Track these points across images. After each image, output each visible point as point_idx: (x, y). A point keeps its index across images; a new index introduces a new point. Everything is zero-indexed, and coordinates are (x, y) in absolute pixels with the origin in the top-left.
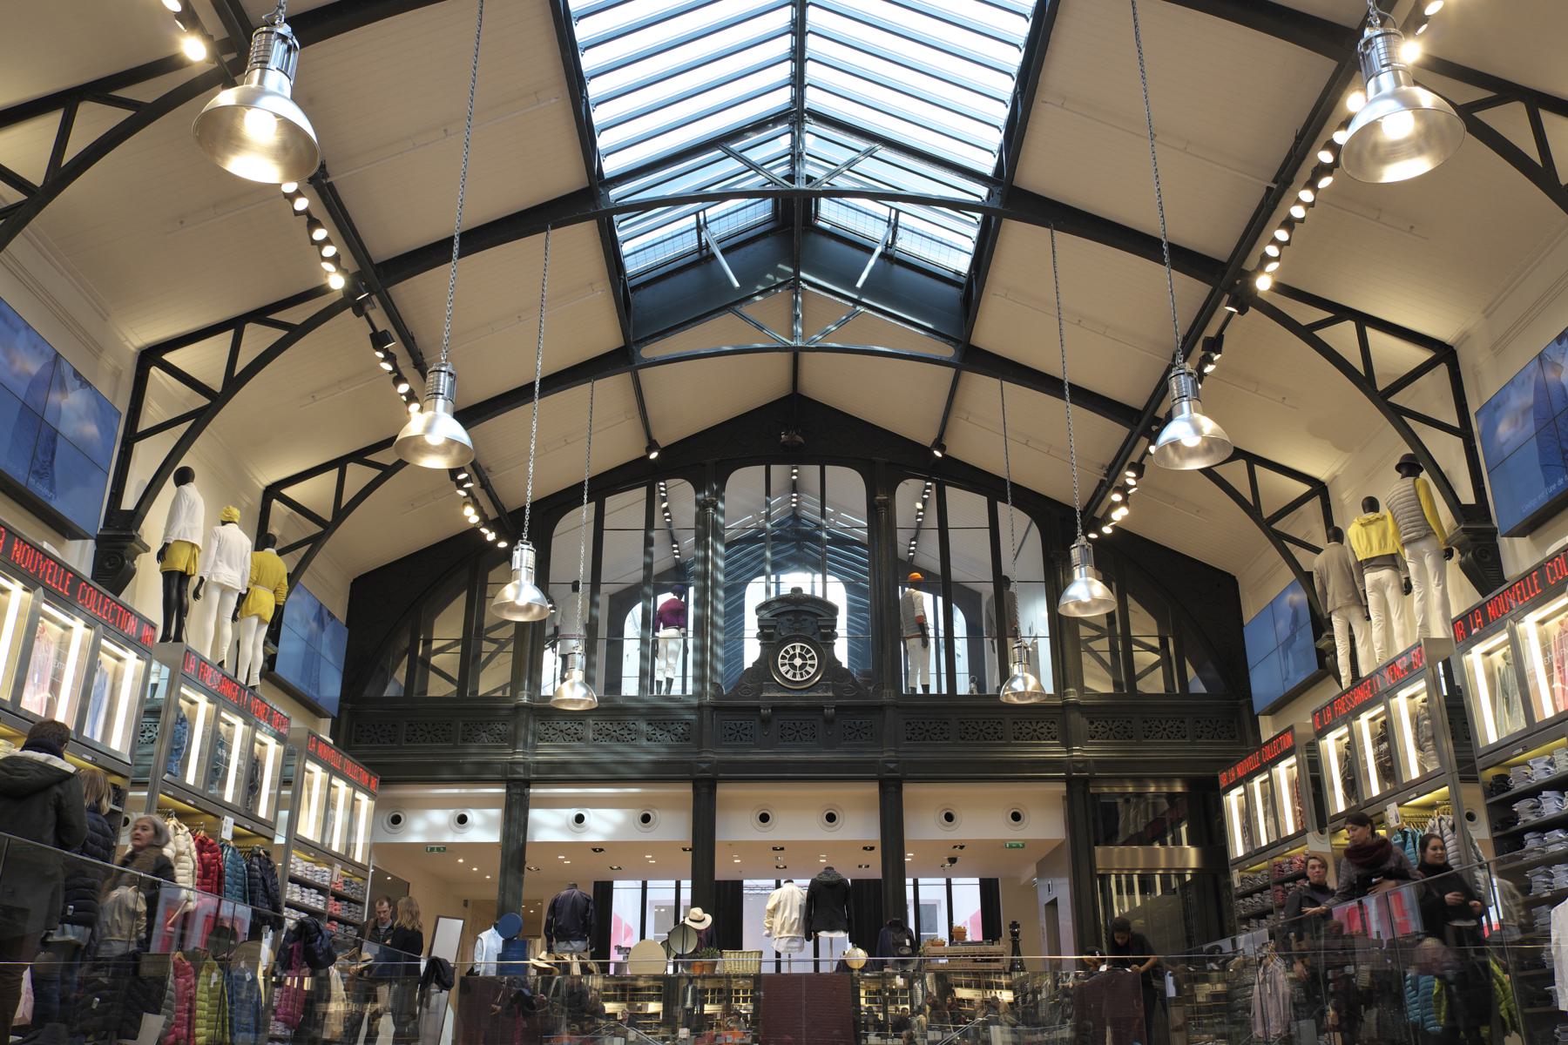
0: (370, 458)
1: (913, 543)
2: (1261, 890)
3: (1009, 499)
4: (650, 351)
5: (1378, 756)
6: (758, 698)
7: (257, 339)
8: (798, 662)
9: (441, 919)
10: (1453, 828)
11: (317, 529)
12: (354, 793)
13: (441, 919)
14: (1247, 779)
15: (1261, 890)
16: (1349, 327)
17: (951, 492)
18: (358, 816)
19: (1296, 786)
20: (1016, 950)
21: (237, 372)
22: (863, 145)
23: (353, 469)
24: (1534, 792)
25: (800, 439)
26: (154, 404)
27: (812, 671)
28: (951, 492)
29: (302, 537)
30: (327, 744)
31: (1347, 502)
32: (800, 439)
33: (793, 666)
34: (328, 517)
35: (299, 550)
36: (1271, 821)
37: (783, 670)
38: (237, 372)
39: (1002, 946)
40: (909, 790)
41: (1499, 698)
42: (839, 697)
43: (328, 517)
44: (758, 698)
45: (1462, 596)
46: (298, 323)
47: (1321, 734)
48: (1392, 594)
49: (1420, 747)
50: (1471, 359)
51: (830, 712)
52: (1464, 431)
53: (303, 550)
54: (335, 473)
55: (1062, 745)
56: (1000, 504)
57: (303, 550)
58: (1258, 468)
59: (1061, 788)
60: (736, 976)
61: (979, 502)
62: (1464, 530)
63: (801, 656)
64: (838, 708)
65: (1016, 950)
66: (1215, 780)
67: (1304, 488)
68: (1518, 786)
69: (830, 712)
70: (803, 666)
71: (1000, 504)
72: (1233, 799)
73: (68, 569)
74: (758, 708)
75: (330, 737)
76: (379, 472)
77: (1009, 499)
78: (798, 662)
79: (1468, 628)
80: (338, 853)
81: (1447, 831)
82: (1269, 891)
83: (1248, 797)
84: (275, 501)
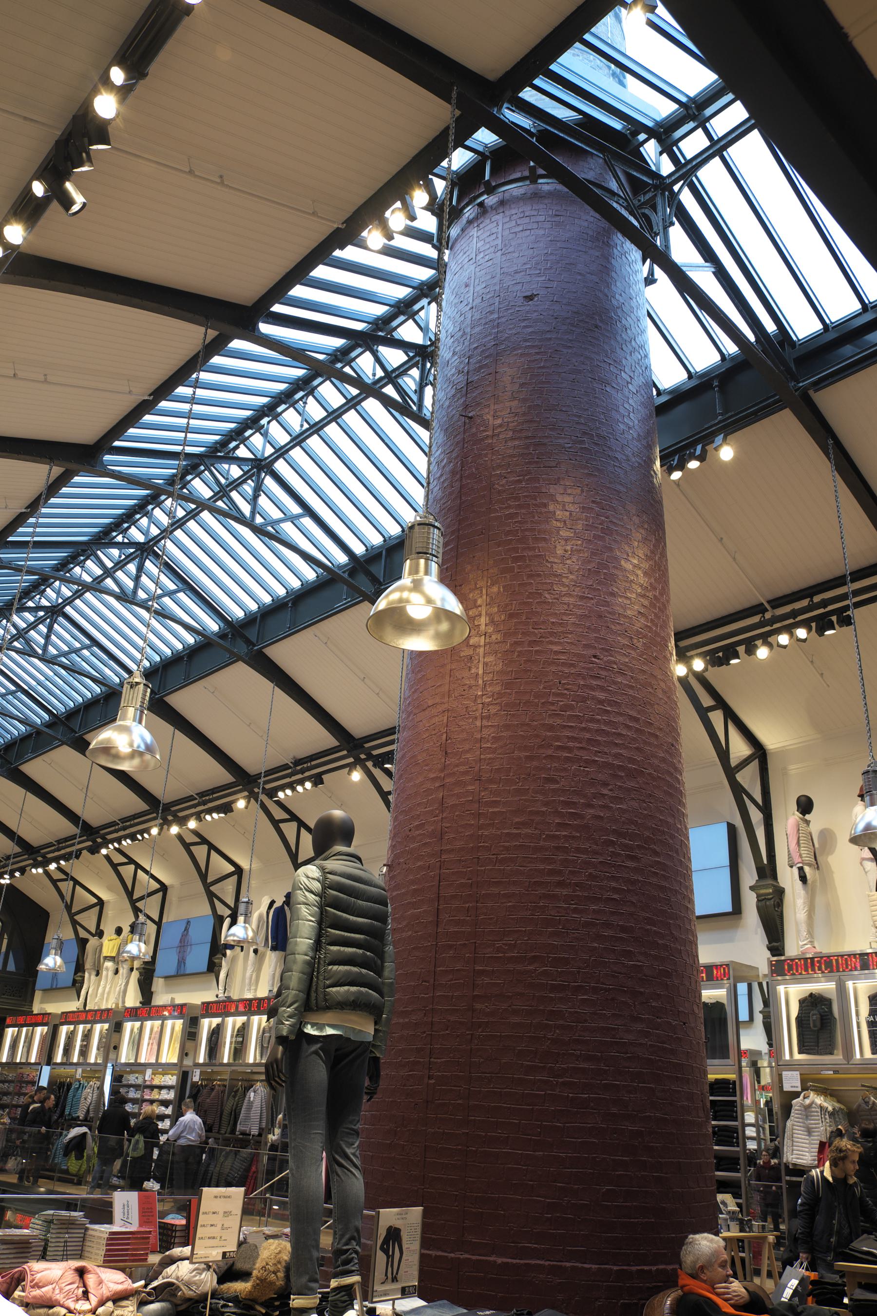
1: (139, 837)
2: (9, 1082)
3: (81, 822)
5: (81, 1046)
9: (729, 908)
10: (98, 1088)
11: (210, 880)
13: (729, 908)
14: (21, 1026)
15: (9, 1082)
16: (205, 848)
19: (43, 1039)
21: (214, 899)
22: (12, 688)
24: (129, 1086)
31: (110, 915)
36: (25, 1049)
38: (214, 899)
41: (131, 1043)
45: (133, 999)
47: (63, 1024)
48: (111, 973)
49: (98, 1049)
50: (172, 896)
52: (159, 924)
58: (213, 852)
62: (144, 968)
66: (4, 1019)
67: (232, 869)
68: (124, 1082)
72: (10, 1032)
77: (81, 822)
79: (133, 1014)
81: (96, 1089)
82: (13, 1084)
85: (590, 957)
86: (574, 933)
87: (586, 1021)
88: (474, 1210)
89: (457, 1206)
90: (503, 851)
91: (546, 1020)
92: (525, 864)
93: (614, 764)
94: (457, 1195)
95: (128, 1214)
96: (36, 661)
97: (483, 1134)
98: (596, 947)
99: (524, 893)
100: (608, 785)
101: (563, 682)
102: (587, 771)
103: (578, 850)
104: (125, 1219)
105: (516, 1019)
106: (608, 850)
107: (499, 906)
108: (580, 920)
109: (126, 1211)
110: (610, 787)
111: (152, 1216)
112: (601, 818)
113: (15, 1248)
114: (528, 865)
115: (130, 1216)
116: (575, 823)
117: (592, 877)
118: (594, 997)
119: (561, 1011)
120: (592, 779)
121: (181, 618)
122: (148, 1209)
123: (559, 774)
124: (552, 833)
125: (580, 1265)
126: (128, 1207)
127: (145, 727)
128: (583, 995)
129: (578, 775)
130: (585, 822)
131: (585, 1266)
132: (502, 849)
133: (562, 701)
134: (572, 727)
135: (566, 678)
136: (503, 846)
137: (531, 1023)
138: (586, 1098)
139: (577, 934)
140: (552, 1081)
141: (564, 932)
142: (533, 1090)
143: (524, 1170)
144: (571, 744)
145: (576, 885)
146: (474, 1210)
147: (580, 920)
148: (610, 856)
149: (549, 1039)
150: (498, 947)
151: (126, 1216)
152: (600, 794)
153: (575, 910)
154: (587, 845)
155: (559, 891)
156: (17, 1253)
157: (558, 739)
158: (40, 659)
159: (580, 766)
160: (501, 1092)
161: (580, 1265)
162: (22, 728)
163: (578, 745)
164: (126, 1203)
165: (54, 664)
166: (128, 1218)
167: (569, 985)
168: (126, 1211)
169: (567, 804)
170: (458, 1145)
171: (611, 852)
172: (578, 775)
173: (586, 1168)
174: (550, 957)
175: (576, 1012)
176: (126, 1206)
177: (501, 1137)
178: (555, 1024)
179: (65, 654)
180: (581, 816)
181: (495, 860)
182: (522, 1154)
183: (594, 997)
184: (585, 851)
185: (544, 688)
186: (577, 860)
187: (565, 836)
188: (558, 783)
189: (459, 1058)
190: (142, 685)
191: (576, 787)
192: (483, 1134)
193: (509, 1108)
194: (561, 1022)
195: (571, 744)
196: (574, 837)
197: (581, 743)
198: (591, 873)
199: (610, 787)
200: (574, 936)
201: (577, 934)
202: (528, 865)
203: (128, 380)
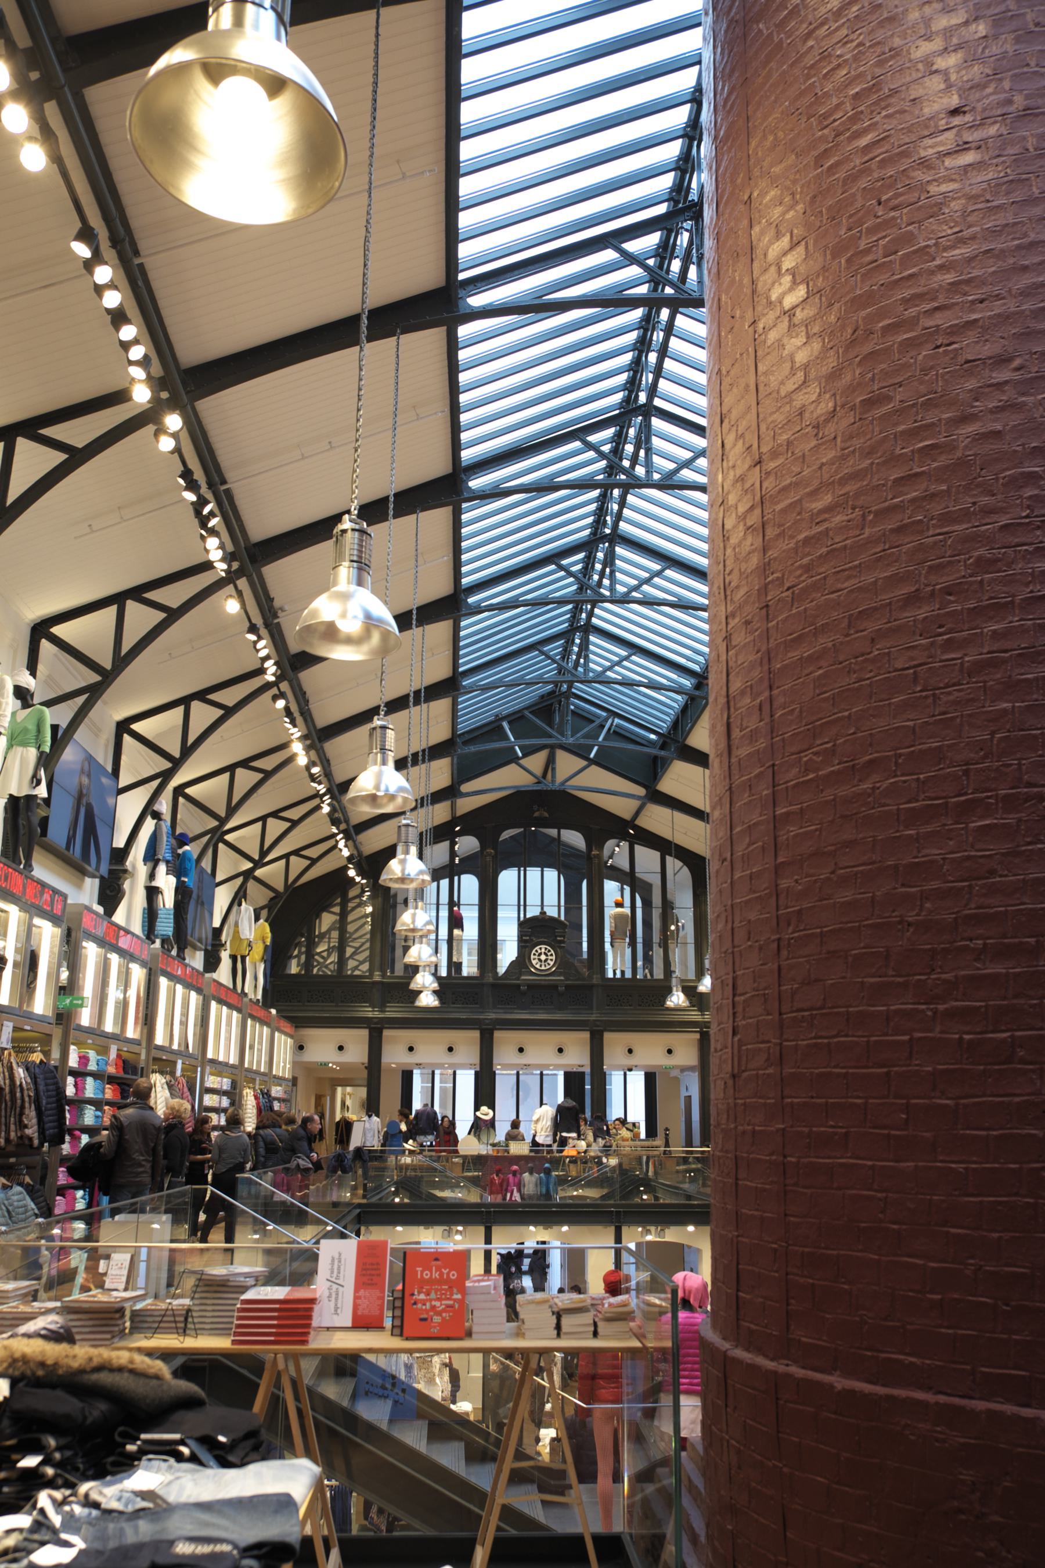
0: (253, 764)
4: (465, 788)
6: (518, 979)
7: (202, 715)
8: (543, 957)
11: (95, 678)
12: (31, 919)
17: (638, 848)
18: (166, 1015)
20: (667, 1145)
23: (240, 772)
25: (546, 815)
26: (164, 802)
27: (552, 963)
28: (638, 848)
29: (152, 773)
30: (96, 913)
32: (546, 815)
33: (540, 960)
34: (107, 664)
35: (76, 699)
37: (534, 962)
39: (659, 1141)
40: (608, 1036)
42: (567, 979)
43: (107, 664)
44: (518, 979)
46: (80, 446)
51: (561, 989)
53: (81, 700)
54: (113, 610)
55: (699, 1010)
56: (667, 857)
57: (81, 700)
59: (698, 1036)
60: (255, 1285)
61: (656, 855)
63: (546, 954)
64: (567, 987)
65: (667, 1145)
69: (561, 989)
70: (546, 960)
71: (667, 857)
73: (221, 985)
74: (519, 986)
75: (100, 903)
76: (64, 456)
78: (543, 957)
80: (43, 1016)
83: (78, 1333)
84: (43, 641)
85: (993, 733)
86: (949, 693)
87: (992, 872)
88: (802, 1280)
89: (776, 1271)
90: (801, 576)
91: (903, 885)
92: (839, 586)
93: (1023, 311)
94: (775, 1250)
95: (339, 1273)
96: (607, 605)
97: (806, 1130)
98: (1005, 710)
99: (841, 643)
100: (1010, 360)
101: (884, 198)
102: (956, 350)
103: (947, 518)
104: (333, 1279)
105: (847, 895)
106: (1021, 497)
107: (803, 683)
108: (962, 664)
109: (336, 1267)
110: (1017, 363)
111: (378, 1275)
112: (997, 434)
113: (91, 1319)
114: (846, 585)
115: (341, 1275)
116: (935, 465)
117: (983, 565)
118: (1010, 819)
119: (932, 862)
120: (967, 362)
121: (695, 482)
122: (372, 1264)
123: (892, 381)
124: (887, 504)
125: (1009, 1409)
126: (340, 1261)
127: (373, 592)
128: (982, 817)
129: (932, 368)
130: (959, 454)
131: (1027, 1412)
132: (799, 572)
133: (885, 237)
134: (911, 276)
135: (890, 187)
136: (800, 567)
137: (873, 897)
138: (1003, 1041)
139: (956, 694)
140: (923, 1011)
141: (926, 697)
142: (887, 1035)
143: (880, 1199)
144: (912, 311)
145: (948, 591)
146: (802, 1280)
147: (962, 664)
148: (1028, 507)
149: (909, 924)
150: (806, 763)
151: (335, 1275)
152: (989, 386)
153: (948, 645)
154: (966, 502)
155: (908, 615)
156: (94, 1326)
157: (881, 314)
158: (612, 602)
159: (938, 347)
160: (829, 1044)
161: (1009, 1409)
162: (679, 697)
163: (928, 307)
164: (336, 1256)
165: (629, 602)
166: (338, 1278)
167: (947, 803)
168: (336, 1267)
169: (913, 434)
170: (772, 1154)
171: (1030, 497)
172: (932, 368)
173: (1016, 1194)
174: (900, 755)
175: (969, 858)
176: (337, 1261)
177: (836, 1134)
178: (922, 892)
179: (636, 588)
180: (950, 447)
181: (790, 599)
182: (872, 1167)
183: (1010, 819)
184: (965, 515)
185: (850, 229)
186: (945, 540)
187: (914, 500)
188: (889, 399)
189: (765, 989)
190: (349, 532)
191: (930, 393)
192: (806, 1130)
193: (846, 1075)
194: (935, 884)
195: (912, 311)
196: (933, 495)
197: (934, 299)
198: (979, 559)
199: (1017, 363)
200: (951, 698)
201: (956, 694)
202: (846, 585)
203: (398, 162)
